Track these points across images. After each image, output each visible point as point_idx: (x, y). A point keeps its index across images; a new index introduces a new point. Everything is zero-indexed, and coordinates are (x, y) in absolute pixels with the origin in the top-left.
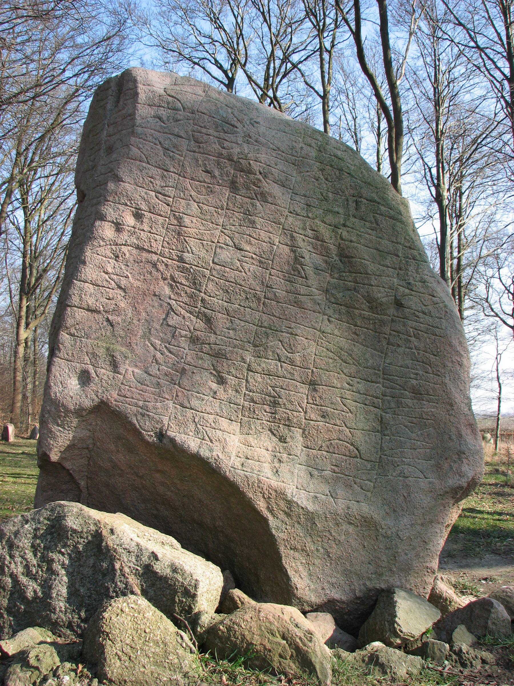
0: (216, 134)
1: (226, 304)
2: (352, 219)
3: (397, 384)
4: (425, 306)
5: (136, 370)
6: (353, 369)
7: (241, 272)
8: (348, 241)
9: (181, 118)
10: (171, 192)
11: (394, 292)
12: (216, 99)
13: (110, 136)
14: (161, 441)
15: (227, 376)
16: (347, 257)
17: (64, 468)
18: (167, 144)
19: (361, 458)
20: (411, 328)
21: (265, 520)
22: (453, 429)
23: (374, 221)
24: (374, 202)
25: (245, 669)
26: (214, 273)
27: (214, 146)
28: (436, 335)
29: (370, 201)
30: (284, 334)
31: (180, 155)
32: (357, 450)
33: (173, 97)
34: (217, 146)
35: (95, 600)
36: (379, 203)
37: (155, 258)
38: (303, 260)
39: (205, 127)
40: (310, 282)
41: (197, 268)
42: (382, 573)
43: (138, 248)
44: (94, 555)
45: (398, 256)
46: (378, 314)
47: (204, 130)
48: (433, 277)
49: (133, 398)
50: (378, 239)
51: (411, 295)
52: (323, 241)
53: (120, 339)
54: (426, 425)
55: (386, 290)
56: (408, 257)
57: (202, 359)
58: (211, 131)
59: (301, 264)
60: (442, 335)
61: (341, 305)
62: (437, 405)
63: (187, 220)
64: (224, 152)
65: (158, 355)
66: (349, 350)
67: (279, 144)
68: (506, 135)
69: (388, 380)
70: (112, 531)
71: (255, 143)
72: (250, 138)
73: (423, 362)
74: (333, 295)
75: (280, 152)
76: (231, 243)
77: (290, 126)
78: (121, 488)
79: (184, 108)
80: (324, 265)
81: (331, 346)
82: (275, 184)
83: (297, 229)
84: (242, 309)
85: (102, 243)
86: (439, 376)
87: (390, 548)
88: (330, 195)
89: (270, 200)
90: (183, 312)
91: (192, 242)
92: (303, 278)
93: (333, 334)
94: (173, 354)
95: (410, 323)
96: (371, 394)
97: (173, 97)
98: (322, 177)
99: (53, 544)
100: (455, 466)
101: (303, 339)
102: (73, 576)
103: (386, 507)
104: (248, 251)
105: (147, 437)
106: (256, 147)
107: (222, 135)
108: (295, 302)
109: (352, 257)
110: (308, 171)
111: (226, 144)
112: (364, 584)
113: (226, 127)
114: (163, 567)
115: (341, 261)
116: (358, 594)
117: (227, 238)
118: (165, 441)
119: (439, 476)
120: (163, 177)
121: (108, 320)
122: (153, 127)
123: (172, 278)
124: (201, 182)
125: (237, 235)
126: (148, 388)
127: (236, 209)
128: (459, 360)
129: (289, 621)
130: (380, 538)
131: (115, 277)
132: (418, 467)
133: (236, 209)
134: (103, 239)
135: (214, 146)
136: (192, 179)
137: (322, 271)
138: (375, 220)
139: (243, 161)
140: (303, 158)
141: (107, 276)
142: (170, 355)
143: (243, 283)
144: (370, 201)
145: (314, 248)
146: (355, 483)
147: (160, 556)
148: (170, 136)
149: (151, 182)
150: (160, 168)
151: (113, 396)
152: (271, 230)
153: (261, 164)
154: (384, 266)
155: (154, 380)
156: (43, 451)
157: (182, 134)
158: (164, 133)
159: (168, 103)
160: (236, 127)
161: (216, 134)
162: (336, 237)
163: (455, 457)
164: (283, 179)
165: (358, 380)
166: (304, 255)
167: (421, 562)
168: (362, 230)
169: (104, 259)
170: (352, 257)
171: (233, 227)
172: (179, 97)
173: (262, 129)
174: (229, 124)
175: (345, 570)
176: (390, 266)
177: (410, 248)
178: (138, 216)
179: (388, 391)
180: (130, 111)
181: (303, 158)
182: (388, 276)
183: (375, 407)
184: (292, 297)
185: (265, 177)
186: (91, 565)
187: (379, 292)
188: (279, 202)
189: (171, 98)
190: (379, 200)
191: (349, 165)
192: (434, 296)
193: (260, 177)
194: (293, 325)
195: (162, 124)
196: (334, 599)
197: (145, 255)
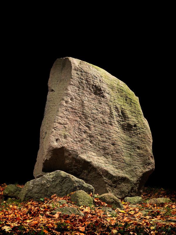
1: (94, 124)
5: (71, 139)
10: (81, 94)
25: (156, 217)
26: (91, 116)
34: (92, 83)
37: (76, 111)
40: (114, 119)
47: (89, 78)
52: (118, 109)
59: (112, 115)
63: (85, 102)
64: (94, 84)
65: (77, 136)
68: (81, 230)
74: (120, 123)
76: (95, 108)
85: (63, 106)
88: (120, 97)
89: (105, 98)
90: (83, 125)
91: (86, 107)
107: (94, 80)
111: (95, 82)
113: (95, 78)
118: (78, 157)
120: (79, 90)
121: (64, 126)
123: (80, 116)
125: (97, 106)
127: (97, 99)
131: (66, 115)
133: (97, 99)
134: (63, 105)
136: (86, 91)
139: (99, 87)
143: (98, 119)
152: (105, 105)
155: (76, 142)
157: (84, 79)
159: (80, 70)
161: (92, 79)
164: (109, 92)
172: (83, 68)
173: (103, 79)
178: (71, 99)
184: (110, 123)
188: (107, 98)
194: (110, 130)
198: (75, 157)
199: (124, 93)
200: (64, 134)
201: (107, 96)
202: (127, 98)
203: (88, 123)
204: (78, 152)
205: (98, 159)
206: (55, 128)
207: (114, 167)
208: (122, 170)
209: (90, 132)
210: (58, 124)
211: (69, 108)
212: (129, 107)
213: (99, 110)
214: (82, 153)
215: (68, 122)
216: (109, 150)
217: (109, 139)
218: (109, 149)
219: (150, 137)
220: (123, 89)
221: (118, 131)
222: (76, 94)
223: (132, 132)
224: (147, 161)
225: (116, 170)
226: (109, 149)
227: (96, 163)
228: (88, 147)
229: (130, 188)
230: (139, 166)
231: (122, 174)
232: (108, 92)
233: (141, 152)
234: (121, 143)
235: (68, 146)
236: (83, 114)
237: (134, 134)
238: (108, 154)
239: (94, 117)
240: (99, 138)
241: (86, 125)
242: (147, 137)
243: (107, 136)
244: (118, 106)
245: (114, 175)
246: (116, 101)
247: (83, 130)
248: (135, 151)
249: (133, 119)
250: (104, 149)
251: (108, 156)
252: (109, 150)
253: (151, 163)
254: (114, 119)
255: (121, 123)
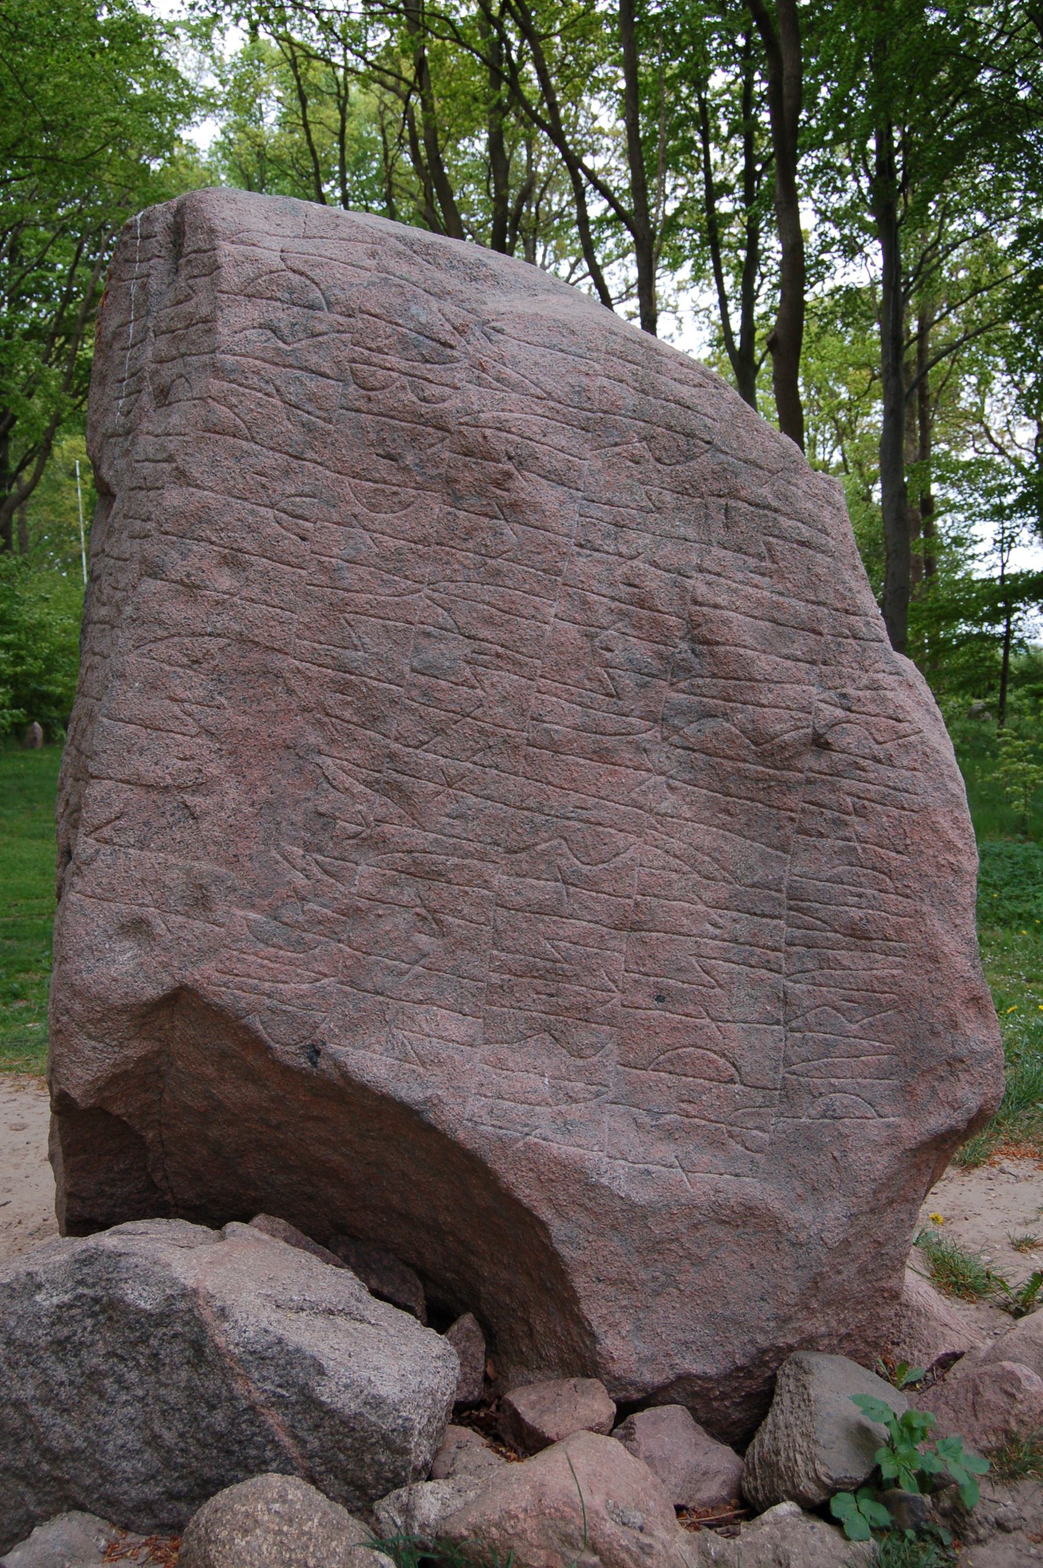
0: (404, 365)
1: (442, 761)
2: (717, 552)
3: (817, 919)
4: (879, 743)
5: (253, 915)
6: (721, 891)
7: (473, 687)
8: (708, 605)
9: (323, 328)
11: (810, 717)
12: (401, 278)
13: (161, 362)
14: (314, 1064)
15: (450, 919)
16: (707, 642)
17: (108, 1114)
18: (293, 393)
19: (742, 1083)
20: (849, 794)
21: (543, 1226)
22: (939, 1012)
23: (766, 554)
24: (765, 507)
27: (402, 396)
28: (904, 809)
29: (757, 505)
30: (572, 823)
31: (324, 419)
32: (734, 1065)
33: (302, 274)
35: (195, 1456)
36: (776, 511)
38: (608, 655)
39: (380, 350)
41: (375, 683)
42: (791, 1318)
43: (241, 639)
44: (188, 1362)
45: (821, 634)
46: (776, 768)
47: (376, 357)
48: (897, 674)
49: (249, 976)
50: (775, 597)
51: (848, 722)
53: (212, 848)
54: (881, 1005)
55: (793, 713)
56: (841, 635)
57: (395, 884)
58: (392, 360)
60: (916, 807)
61: (694, 751)
62: (904, 961)
66: (715, 850)
67: (550, 384)
69: (799, 910)
70: (223, 1314)
71: (496, 384)
72: (484, 370)
73: (874, 869)
74: (677, 730)
75: (552, 404)
77: (573, 332)
78: (234, 1146)
79: (328, 303)
80: (655, 663)
81: (676, 845)
82: (544, 481)
83: (595, 585)
84: (477, 769)
86: (908, 897)
87: (805, 1266)
88: (668, 497)
90: (349, 781)
92: (612, 696)
93: (679, 817)
94: (332, 876)
95: (845, 783)
96: (761, 943)
97: (302, 274)
98: (648, 455)
99: (98, 1337)
100: (941, 1087)
101: (613, 831)
102: (147, 1405)
103: (796, 1184)
104: (487, 641)
105: (286, 1057)
106: (500, 395)
107: (424, 369)
108: (595, 752)
109: (718, 643)
110: (616, 445)
112: (753, 1341)
114: (334, 1389)
115: (693, 651)
116: (740, 1361)
117: (440, 610)
118: (323, 1064)
119: (908, 1109)
122: (258, 353)
124: (376, 482)
126: (281, 952)
128: (952, 860)
129: (603, 1513)
130: (785, 1246)
132: (863, 1095)
134: (161, 623)
135: (402, 396)
137: (654, 676)
138: (769, 550)
140: (605, 412)
141: (176, 709)
142: (325, 877)
143: (478, 712)
144: (757, 505)
145: (634, 626)
146: (731, 1137)
147: (328, 1364)
148: (298, 373)
149: (263, 486)
150: (280, 451)
151: (203, 974)
153: (509, 436)
154: (788, 658)
156: (61, 1090)
158: (285, 366)
160: (452, 347)
162: (682, 598)
163: (942, 1071)
165: (735, 914)
166: (612, 645)
167: (870, 1282)
168: (740, 576)
169: (167, 668)
170: (718, 643)
171: (453, 586)
172: (316, 274)
173: (511, 348)
174: (433, 340)
175: (710, 1315)
176: (802, 657)
177: (847, 612)
179: (798, 933)
180: (205, 311)
181: (605, 412)
182: (799, 682)
183: (771, 970)
184: (589, 740)
185: (521, 465)
186: (183, 1385)
187: (780, 720)
189: (298, 277)
190: (775, 504)
191: (709, 422)
192: (899, 721)
193: (509, 466)
195: (281, 345)
196: (690, 1374)
197: (255, 655)
198: (303, 1062)
199: (706, 462)
200: (188, 872)
201: (551, 507)
202: (732, 503)
203: (392, 756)
204: (319, 1015)
205: (500, 1065)
206: (107, 832)
207: (639, 1126)
208: (716, 1143)
209: (420, 838)
210: (128, 793)
211: (213, 645)
212: (757, 579)
213: (485, 633)
214: (351, 1027)
215: (213, 770)
216: (588, 980)
217: (591, 884)
218: (592, 971)
219: (953, 835)
220: (695, 423)
221: (664, 807)
222: (270, 513)
223: (793, 800)
224: (933, 1043)
225: (666, 1151)
226: (592, 971)
227: (475, 1106)
228: (402, 974)
229: (793, 1286)
230: (867, 1095)
231: (709, 1178)
232: (557, 462)
233: (885, 967)
234: (701, 907)
235: (230, 972)
236: (343, 688)
237: (808, 823)
238: (585, 1014)
239: (438, 704)
240: (500, 879)
241: (377, 781)
242: (929, 836)
243: (570, 862)
244: (654, 581)
245: (642, 1195)
246: (632, 535)
247: (353, 828)
248: (824, 963)
249: (791, 690)
250: (550, 973)
251: (583, 1036)
252: (588, 980)
253: (972, 1052)
254: (626, 704)
255: (690, 730)
